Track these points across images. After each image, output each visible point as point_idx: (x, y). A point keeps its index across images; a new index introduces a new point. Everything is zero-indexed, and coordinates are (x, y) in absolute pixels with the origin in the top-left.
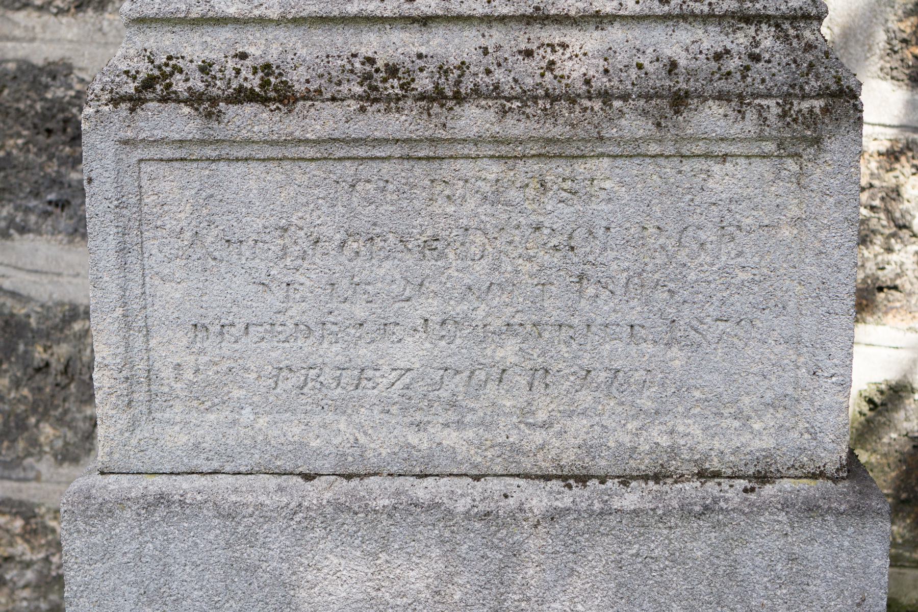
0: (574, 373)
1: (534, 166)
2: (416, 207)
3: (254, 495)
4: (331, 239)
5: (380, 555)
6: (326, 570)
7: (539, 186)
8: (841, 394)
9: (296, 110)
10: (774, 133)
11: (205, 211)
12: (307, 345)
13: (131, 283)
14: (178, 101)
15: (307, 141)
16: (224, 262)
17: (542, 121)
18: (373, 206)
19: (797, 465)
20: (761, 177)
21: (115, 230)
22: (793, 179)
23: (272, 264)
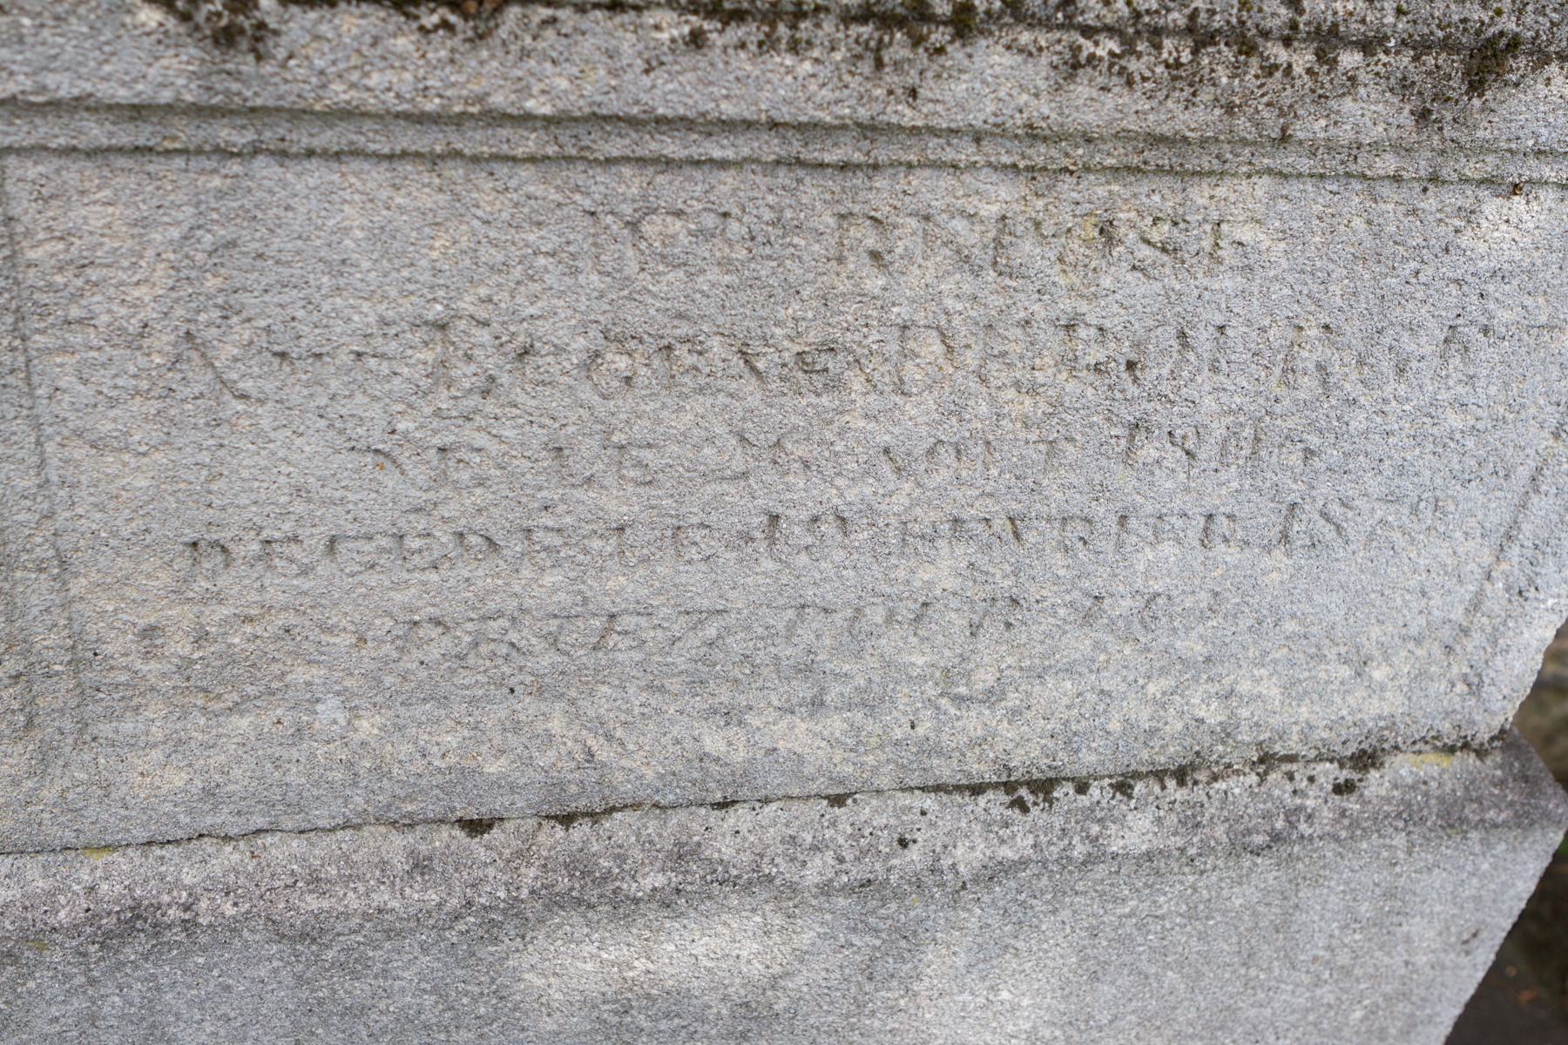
1: (1099, 190)
2: (791, 278)
3: (361, 889)
4: (559, 350)
9: (503, 32)
11: (212, 283)
12: (482, 575)
15: (526, 119)
16: (270, 404)
17: (1161, 95)
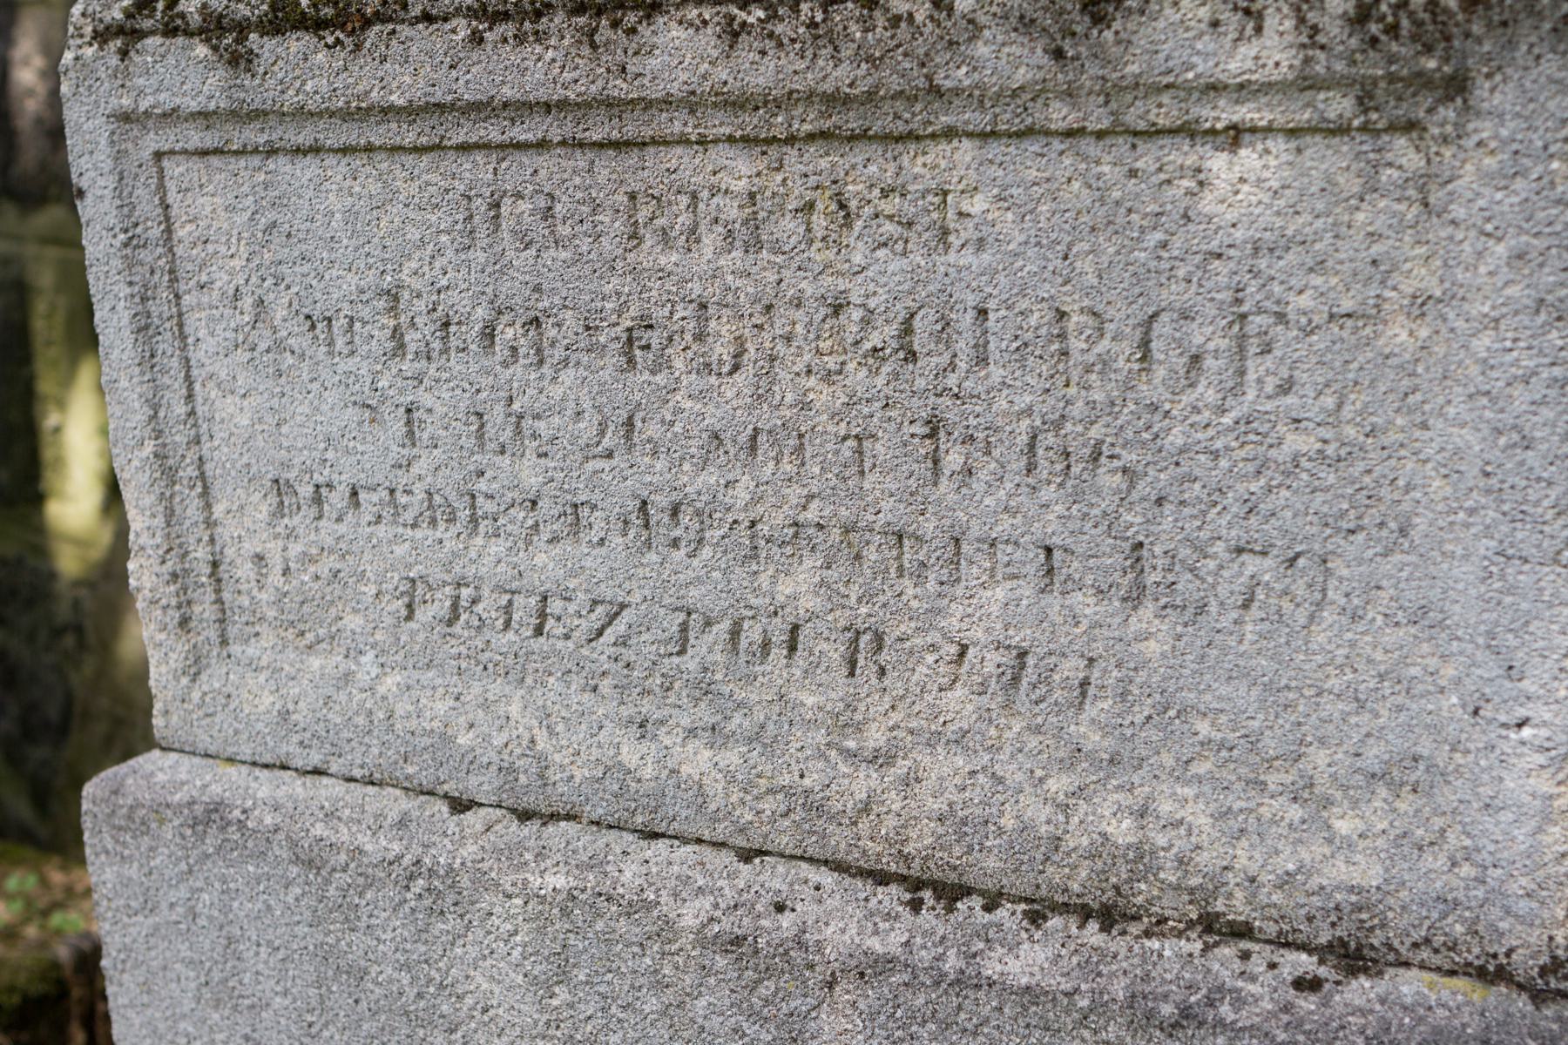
0: (933, 648)
1: (822, 161)
5: (557, 990)
6: (469, 1001)
7: (833, 207)
8: (1546, 774)
9: (367, 44)
10: (1339, 67)
13: (168, 394)
14: (189, 34)
17: (809, 54)
18: (533, 252)
19: (1438, 940)
20: (1329, 187)
21: (128, 290)
22: (1411, 192)
23: (379, 367)
